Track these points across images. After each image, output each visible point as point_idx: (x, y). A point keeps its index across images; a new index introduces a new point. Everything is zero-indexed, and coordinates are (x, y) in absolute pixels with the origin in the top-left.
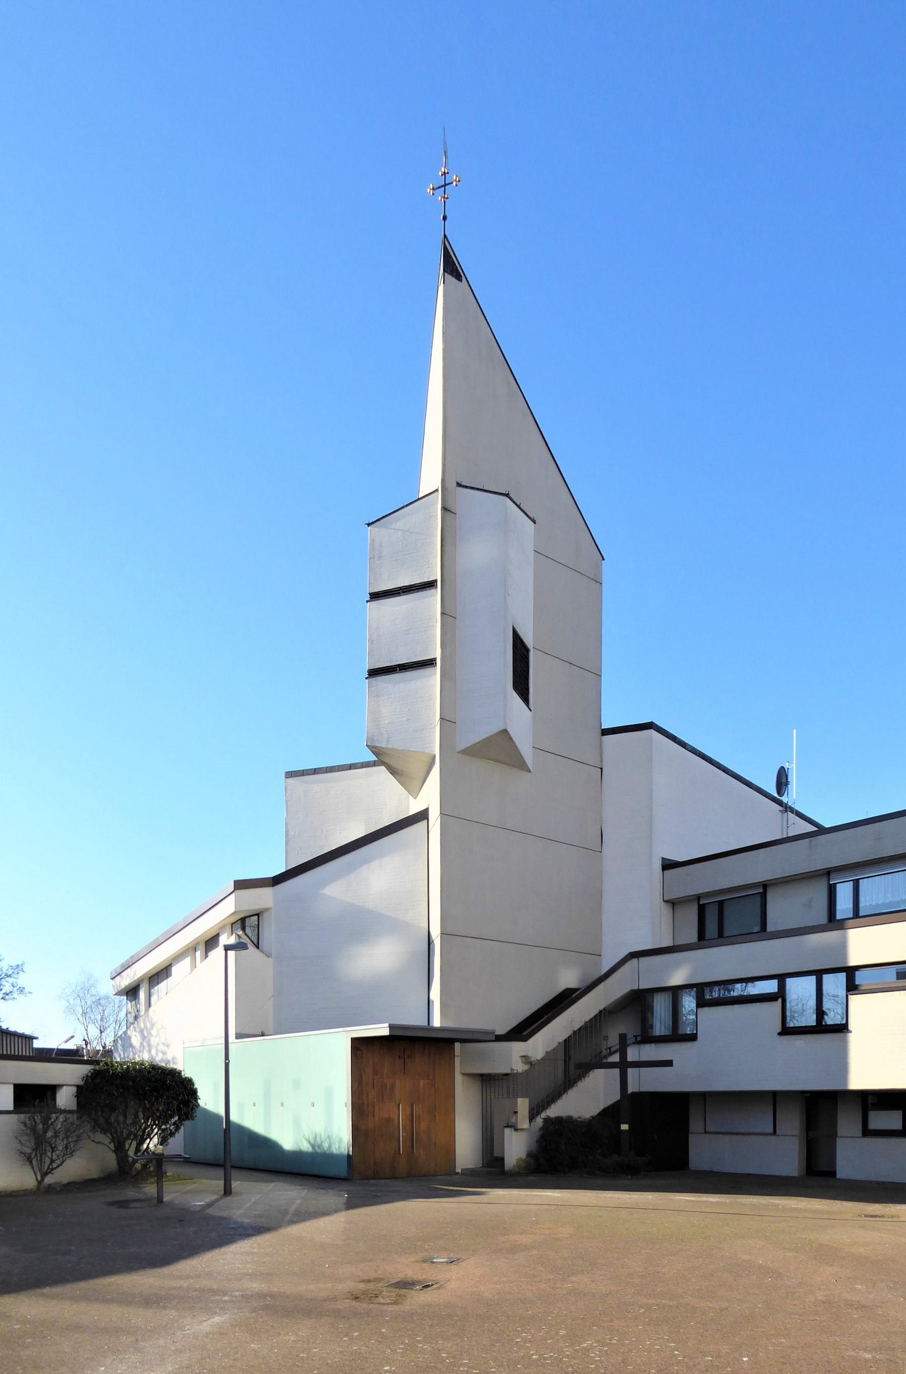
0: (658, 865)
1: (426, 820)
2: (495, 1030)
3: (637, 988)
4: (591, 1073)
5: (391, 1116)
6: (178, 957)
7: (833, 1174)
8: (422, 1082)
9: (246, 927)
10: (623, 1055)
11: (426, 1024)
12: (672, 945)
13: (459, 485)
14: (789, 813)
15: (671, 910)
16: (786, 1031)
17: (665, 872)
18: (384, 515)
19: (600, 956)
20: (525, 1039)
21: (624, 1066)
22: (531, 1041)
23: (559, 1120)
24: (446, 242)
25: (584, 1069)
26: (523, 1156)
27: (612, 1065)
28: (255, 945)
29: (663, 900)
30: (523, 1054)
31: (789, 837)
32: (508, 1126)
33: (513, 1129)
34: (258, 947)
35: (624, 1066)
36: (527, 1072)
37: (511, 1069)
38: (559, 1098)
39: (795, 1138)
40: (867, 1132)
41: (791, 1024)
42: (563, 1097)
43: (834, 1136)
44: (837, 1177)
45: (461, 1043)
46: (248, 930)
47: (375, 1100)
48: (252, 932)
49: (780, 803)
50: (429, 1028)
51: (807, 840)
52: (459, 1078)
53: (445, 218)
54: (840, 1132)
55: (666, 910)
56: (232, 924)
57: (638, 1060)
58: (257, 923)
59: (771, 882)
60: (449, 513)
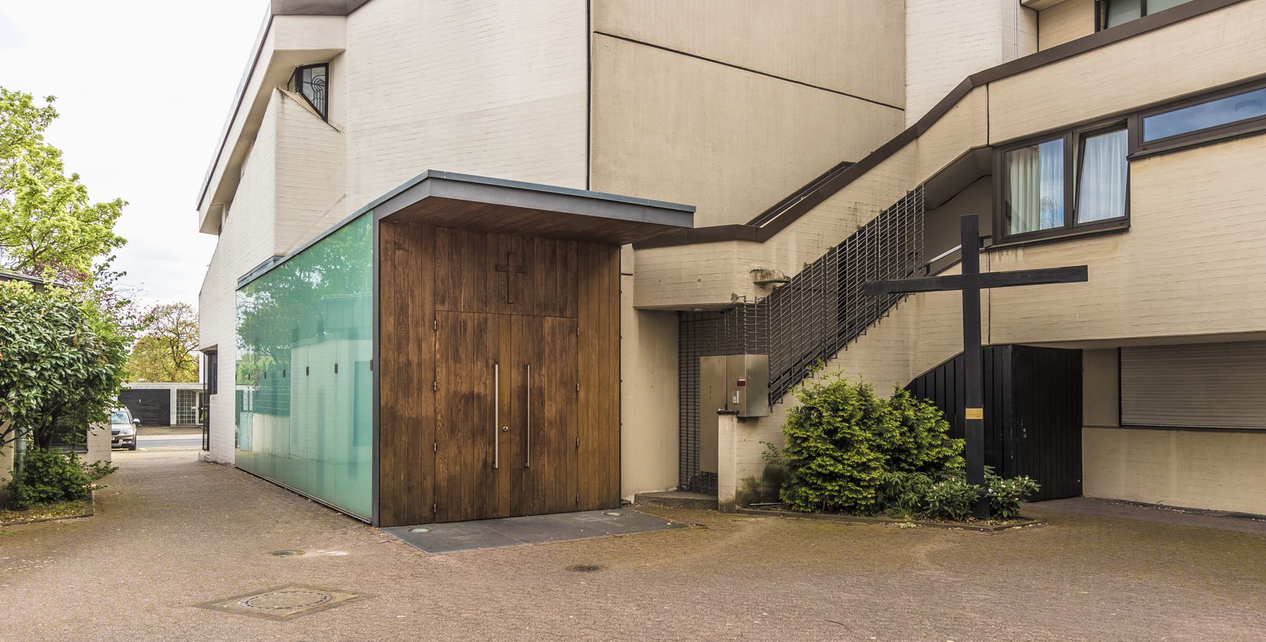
5: (476, 390)
8: (548, 322)
9: (305, 85)
12: (1036, 52)
19: (903, 110)
21: (972, 284)
22: (774, 243)
26: (758, 476)
27: (950, 284)
28: (318, 112)
30: (756, 266)
31: (992, 146)
33: (735, 420)
34: (325, 118)
35: (972, 284)
36: (762, 305)
37: (733, 295)
46: (307, 90)
48: (315, 92)
52: (629, 322)
58: (323, 78)
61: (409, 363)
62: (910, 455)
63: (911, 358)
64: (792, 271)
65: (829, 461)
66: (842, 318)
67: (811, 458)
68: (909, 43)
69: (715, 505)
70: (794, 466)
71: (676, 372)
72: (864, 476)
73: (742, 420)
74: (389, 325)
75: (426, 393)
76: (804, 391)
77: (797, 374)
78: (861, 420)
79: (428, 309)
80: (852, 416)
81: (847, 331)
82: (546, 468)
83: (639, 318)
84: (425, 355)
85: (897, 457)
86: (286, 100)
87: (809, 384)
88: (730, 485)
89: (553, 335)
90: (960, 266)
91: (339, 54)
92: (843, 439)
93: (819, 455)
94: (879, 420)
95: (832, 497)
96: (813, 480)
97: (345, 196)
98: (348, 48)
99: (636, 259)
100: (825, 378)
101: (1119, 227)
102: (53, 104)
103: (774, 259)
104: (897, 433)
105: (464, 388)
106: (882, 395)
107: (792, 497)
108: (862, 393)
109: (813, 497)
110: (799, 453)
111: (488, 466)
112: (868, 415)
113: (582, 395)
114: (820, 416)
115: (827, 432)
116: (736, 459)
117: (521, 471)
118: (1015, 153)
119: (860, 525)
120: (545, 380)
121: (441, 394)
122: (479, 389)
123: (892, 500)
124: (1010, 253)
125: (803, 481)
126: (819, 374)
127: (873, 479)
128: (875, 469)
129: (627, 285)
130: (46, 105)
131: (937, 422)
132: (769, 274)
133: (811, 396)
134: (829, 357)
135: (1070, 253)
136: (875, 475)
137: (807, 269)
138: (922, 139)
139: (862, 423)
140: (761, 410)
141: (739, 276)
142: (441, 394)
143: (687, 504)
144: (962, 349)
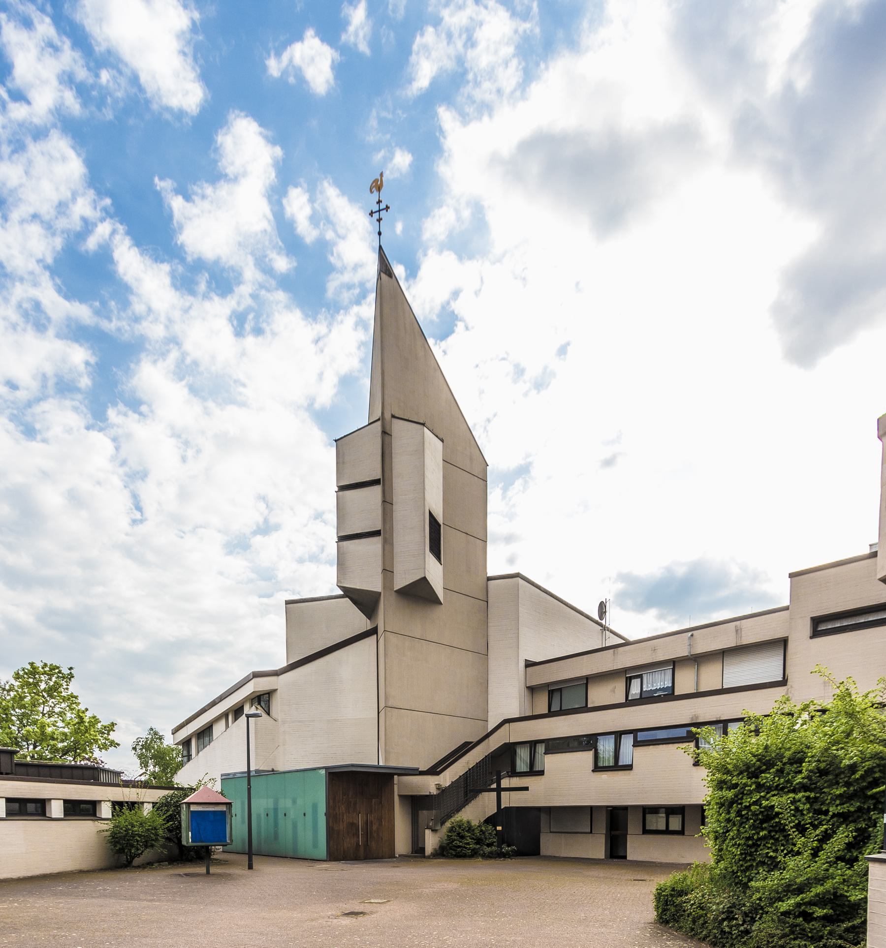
0: (522, 664)
1: (376, 635)
2: (419, 768)
3: (508, 742)
4: (480, 795)
6: (217, 719)
7: (625, 857)
8: (374, 800)
9: (262, 702)
10: (499, 784)
11: (377, 764)
13: (393, 416)
14: (607, 631)
16: (597, 768)
18: (345, 435)
20: (438, 774)
21: (499, 790)
22: (442, 775)
26: (437, 848)
28: (267, 712)
29: (527, 687)
30: (436, 783)
32: (427, 828)
34: (269, 714)
40: (645, 832)
41: (600, 764)
42: (462, 810)
43: (626, 834)
44: (628, 859)
45: (398, 776)
46: (262, 704)
48: (265, 704)
49: (600, 625)
51: (612, 650)
52: (396, 798)
56: (252, 700)
58: (268, 699)
59: (591, 676)
61: (336, 813)
62: (483, 841)
63: (486, 810)
64: (448, 784)
67: (453, 841)
69: (424, 857)
70: (448, 844)
71: (411, 815)
72: (468, 846)
73: (432, 830)
74: (331, 804)
75: (341, 823)
76: (451, 822)
77: (449, 816)
79: (341, 797)
80: (464, 829)
82: (373, 845)
83: (400, 799)
84: (340, 811)
85: (479, 841)
87: (452, 820)
88: (429, 850)
91: (276, 690)
92: (462, 835)
94: (473, 830)
95: (459, 853)
96: (454, 848)
97: (279, 746)
99: (398, 779)
101: (629, 767)
103: (442, 780)
104: (478, 834)
105: (351, 821)
106: (475, 823)
109: (454, 853)
110: (450, 840)
111: (358, 844)
112: (470, 829)
113: (383, 823)
114: (456, 829)
115: (457, 834)
117: (366, 845)
118: (518, 746)
119: (467, 861)
120: (373, 818)
121: (345, 823)
122: (355, 821)
123: (476, 853)
124: (515, 778)
126: (456, 816)
127: (471, 847)
130: (69, 672)
131: (492, 831)
132: (441, 786)
133: (453, 823)
134: (459, 811)
135: (530, 780)
136: (471, 846)
137: (452, 782)
140: (438, 828)
141: (431, 786)
142: (345, 823)
143: (415, 857)
144: (496, 811)
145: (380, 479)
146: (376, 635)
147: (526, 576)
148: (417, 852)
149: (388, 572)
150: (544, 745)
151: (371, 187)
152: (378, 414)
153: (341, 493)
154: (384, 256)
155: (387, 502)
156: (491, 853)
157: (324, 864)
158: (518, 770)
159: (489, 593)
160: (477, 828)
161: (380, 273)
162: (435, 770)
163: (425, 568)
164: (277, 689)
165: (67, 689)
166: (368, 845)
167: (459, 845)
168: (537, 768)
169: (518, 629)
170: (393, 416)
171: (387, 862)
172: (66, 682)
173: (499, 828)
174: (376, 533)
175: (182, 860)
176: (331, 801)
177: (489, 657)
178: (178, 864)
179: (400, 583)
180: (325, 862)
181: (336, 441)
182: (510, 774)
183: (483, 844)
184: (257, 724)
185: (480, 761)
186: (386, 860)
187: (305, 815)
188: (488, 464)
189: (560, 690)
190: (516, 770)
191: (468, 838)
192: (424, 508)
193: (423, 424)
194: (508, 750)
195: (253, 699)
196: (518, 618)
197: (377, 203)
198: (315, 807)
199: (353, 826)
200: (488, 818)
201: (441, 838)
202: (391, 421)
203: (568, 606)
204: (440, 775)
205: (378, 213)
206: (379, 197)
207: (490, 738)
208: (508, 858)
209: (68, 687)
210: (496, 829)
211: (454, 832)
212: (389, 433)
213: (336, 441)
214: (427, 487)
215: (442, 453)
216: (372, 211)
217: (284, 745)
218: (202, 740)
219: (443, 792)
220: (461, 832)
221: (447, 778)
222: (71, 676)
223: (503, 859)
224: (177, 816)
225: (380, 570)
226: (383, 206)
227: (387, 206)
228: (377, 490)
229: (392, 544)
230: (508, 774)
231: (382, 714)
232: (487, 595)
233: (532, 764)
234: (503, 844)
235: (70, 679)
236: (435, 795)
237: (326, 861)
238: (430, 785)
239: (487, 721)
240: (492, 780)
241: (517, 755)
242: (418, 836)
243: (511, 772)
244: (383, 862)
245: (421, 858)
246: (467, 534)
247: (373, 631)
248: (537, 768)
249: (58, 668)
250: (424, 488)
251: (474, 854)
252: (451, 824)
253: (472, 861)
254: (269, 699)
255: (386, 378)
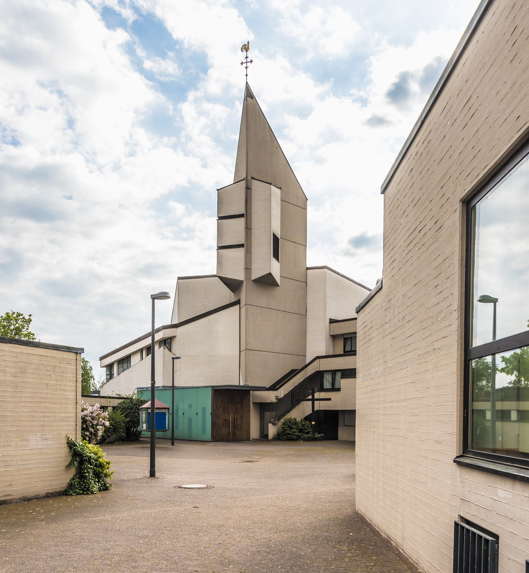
0: (328, 321)
1: (239, 305)
4: (301, 403)
8: (238, 406)
10: (313, 396)
13: (253, 178)
15: (333, 340)
17: (331, 324)
20: (277, 390)
21: (313, 400)
22: (279, 390)
23: (290, 421)
24: (248, 85)
25: (299, 402)
26: (276, 434)
27: (309, 400)
28: (169, 349)
30: (276, 395)
32: (270, 423)
34: (170, 351)
36: (277, 402)
38: (297, 405)
39: (520, 425)
42: (291, 412)
46: (167, 345)
47: (222, 413)
50: (239, 386)
53: (247, 75)
54: (339, 425)
55: (330, 339)
56: (160, 342)
57: (319, 398)
58: (170, 342)
60: (248, 189)
61: (217, 414)
62: (303, 431)
64: (282, 396)
65: (289, 431)
66: (291, 404)
67: (285, 431)
68: (307, 341)
69: (268, 440)
70: (282, 432)
73: (273, 424)
76: (284, 419)
77: (283, 415)
78: (294, 424)
79: (220, 404)
80: (292, 423)
81: (293, 406)
82: (238, 433)
85: (301, 431)
86: (165, 349)
87: (285, 417)
88: (271, 436)
89: (239, 408)
90: (311, 396)
93: (287, 430)
94: (298, 424)
97: (176, 371)
98: (177, 335)
100: (288, 416)
102: (31, 317)
104: (301, 426)
105: (225, 418)
106: (299, 419)
107: (282, 438)
108: (295, 419)
109: (286, 438)
111: (229, 432)
112: (296, 423)
113: (244, 419)
114: (287, 423)
115: (288, 426)
116: (272, 431)
117: (234, 433)
118: (325, 373)
119: (294, 442)
121: (222, 419)
122: (228, 418)
123: (299, 438)
125: (284, 435)
127: (296, 434)
128: (296, 433)
129: (251, 397)
131: (309, 425)
132: (278, 397)
133: (285, 420)
135: (332, 393)
136: (296, 433)
137: (285, 395)
138: (308, 367)
139: (294, 425)
142: (222, 419)
143: (262, 440)
144: (311, 412)
145: (244, 214)
146: (239, 305)
147: (330, 267)
148: (264, 437)
149: (248, 269)
150: (340, 372)
151: (241, 49)
152: (244, 176)
153: (220, 221)
154: (249, 87)
155: (248, 228)
156: (308, 438)
157: (211, 444)
158: (325, 387)
159: (307, 277)
160: (300, 423)
161: (246, 97)
162: (274, 387)
163: (270, 268)
164: (176, 336)
165: (27, 329)
166: (235, 432)
167: (289, 433)
168: (336, 386)
169: (326, 300)
170: (253, 178)
171: (245, 442)
172: (27, 324)
173: (313, 423)
174: (242, 246)
175: (128, 440)
176: (215, 407)
177: (307, 316)
178: (127, 442)
179: (255, 276)
180: (210, 443)
181: (217, 190)
182: (320, 389)
183: (304, 432)
184: (164, 358)
185: (302, 382)
186: (244, 442)
187: (197, 414)
188: (308, 199)
189: (351, 338)
190: (323, 387)
191: (295, 429)
192: (271, 232)
193: (271, 184)
194: (319, 375)
195: (161, 342)
196: (326, 293)
197: (245, 58)
198: (204, 409)
199: (226, 421)
200: (306, 417)
201: (278, 429)
202: (251, 181)
203: (356, 284)
204: (278, 391)
205: (247, 61)
206: (247, 55)
207: (308, 367)
208: (319, 441)
209: (28, 328)
210: (311, 423)
211: (286, 425)
212: (250, 188)
213: (217, 190)
214: (272, 220)
215: (280, 196)
216: (242, 62)
217: (180, 370)
218: (122, 365)
219: (279, 400)
220: (291, 424)
221: (282, 392)
222: (30, 320)
223: (315, 441)
224: (129, 415)
225: (243, 268)
226: (249, 60)
227: (251, 60)
228: (242, 220)
229: (251, 253)
230: (319, 390)
231: (243, 353)
232: (307, 279)
233: (333, 384)
234: (315, 433)
235: (29, 323)
236: (275, 403)
237: (211, 442)
238: (271, 397)
239: (306, 356)
240: (309, 393)
241: (324, 377)
242: (264, 428)
243: (320, 388)
244: (243, 442)
245: (266, 441)
246: (295, 243)
247: (238, 302)
248: (336, 386)
249: (22, 315)
250: (271, 221)
251: (298, 439)
252: (284, 420)
253: (297, 442)
254: (171, 342)
255: (249, 156)
